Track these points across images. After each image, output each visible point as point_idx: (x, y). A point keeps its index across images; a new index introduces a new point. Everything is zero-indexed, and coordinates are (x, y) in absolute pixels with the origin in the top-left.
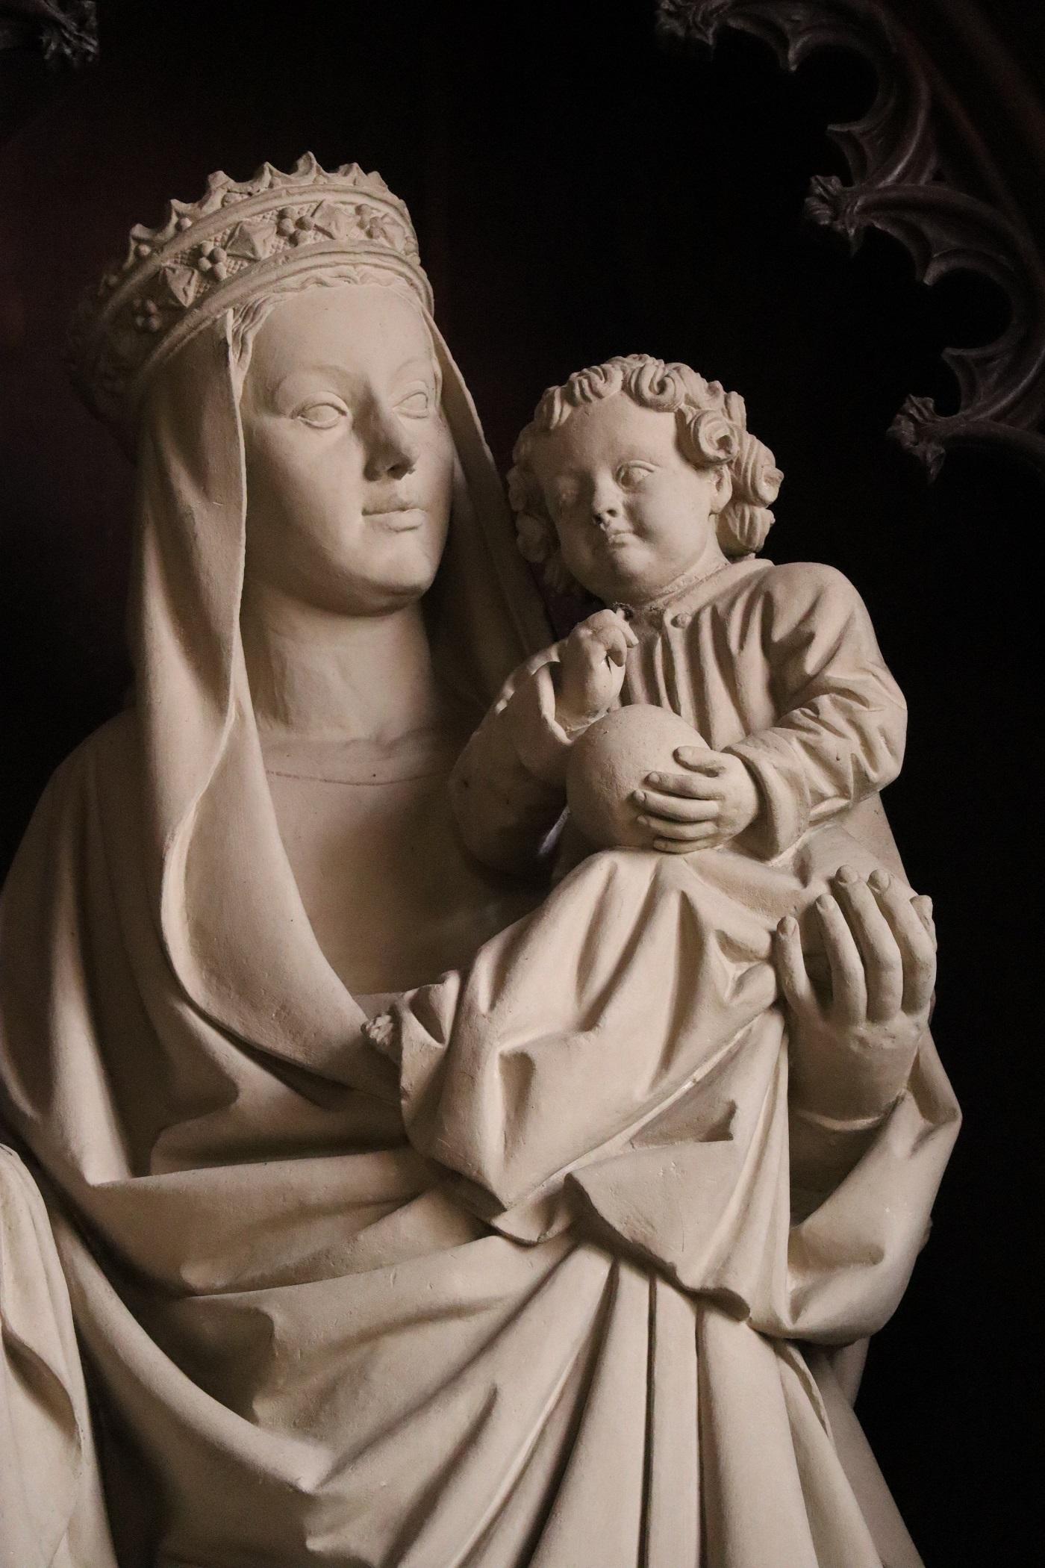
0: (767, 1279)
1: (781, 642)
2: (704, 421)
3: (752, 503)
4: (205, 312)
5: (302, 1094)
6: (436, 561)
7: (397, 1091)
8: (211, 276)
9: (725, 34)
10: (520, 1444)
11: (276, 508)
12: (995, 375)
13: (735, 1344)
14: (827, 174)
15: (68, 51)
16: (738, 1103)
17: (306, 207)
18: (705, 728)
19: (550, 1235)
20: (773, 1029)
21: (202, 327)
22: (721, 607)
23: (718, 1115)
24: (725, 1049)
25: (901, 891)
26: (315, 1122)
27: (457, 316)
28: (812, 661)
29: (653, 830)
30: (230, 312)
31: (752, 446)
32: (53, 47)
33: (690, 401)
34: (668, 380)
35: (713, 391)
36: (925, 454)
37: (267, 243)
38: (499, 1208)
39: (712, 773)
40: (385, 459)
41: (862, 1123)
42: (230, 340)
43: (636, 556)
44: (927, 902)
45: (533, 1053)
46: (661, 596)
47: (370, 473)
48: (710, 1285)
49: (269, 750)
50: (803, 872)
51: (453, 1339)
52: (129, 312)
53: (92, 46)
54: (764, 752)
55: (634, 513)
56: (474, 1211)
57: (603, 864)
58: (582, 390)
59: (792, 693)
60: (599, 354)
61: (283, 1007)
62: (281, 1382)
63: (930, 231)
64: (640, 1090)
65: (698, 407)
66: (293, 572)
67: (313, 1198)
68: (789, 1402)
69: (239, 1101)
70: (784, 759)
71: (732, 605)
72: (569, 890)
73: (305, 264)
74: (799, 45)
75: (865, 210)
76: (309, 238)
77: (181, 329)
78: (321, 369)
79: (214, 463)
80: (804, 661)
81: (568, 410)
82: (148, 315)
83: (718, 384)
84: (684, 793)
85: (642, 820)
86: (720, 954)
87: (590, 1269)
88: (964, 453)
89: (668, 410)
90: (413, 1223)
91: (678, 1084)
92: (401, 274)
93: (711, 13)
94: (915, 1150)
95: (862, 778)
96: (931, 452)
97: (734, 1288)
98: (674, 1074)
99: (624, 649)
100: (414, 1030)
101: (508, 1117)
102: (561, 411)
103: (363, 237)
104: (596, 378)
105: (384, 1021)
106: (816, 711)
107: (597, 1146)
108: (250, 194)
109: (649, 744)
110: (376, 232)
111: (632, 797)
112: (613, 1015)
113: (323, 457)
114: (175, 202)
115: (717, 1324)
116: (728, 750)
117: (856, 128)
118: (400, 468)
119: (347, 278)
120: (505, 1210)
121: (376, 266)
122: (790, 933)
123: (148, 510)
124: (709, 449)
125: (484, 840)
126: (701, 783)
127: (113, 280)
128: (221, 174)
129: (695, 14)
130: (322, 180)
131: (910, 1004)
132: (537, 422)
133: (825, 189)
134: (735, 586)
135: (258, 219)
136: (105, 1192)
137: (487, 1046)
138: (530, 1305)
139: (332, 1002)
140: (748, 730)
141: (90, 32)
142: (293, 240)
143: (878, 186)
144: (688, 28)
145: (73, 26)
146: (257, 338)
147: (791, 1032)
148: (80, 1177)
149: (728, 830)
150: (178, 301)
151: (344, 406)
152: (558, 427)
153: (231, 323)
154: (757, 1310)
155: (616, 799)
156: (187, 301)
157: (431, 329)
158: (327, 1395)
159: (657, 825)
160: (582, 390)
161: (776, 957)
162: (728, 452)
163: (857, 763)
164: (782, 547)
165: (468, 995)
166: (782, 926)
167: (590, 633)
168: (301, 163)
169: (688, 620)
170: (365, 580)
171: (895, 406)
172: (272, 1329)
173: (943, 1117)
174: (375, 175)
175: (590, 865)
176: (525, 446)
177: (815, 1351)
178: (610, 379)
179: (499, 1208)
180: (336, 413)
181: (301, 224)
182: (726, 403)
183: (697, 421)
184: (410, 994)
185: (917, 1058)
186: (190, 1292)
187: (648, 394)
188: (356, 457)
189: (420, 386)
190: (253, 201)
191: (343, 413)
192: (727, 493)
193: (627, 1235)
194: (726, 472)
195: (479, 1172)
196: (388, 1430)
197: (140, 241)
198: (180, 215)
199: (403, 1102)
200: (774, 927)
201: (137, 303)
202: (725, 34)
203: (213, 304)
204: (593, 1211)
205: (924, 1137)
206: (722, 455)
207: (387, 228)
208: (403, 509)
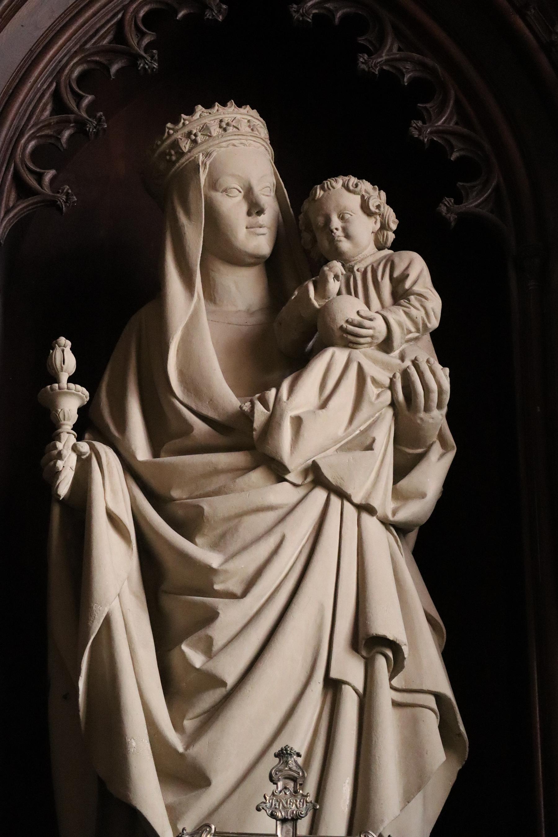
0: (383, 501)
1: (397, 277)
2: (371, 199)
3: (387, 230)
4: (192, 154)
5: (215, 430)
6: (272, 248)
7: (252, 429)
8: (195, 142)
9: (382, 71)
10: (293, 555)
11: (214, 223)
12: (475, 193)
13: (371, 524)
14: (417, 119)
15: (147, 67)
16: (376, 438)
17: (230, 119)
18: (367, 303)
19: (306, 482)
20: (390, 413)
21: (191, 159)
22: (375, 265)
23: (368, 442)
24: (372, 419)
25: (438, 367)
26: (221, 440)
27: (281, 162)
28: (408, 284)
29: (348, 339)
30: (201, 155)
31: (388, 210)
32: (142, 65)
33: (366, 192)
34: (359, 183)
35: (374, 189)
36: (450, 217)
37: (215, 130)
38: (287, 471)
39: (371, 320)
40: (254, 208)
41: (420, 451)
42: (200, 164)
43: (345, 245)
44: (447, 370)
45: (302, 416)
46: (353, 261)
47: (249, 214)
48: (363, 502)
49: (208, 312)
50: (402, 358)
51: (270, 517)
52: (164, 154)
53: (156, 65)
54: (389, 315)
55: (345, 230)
56: (278, 472)
57: (330, 351)
58: (327, 185)
59: (400, 295)
60: (335, 174)
61: (211, 400)
62: (206, 531)
63: (454, 142)
64: (341, 432)
65: (369, 194)
66: (221, 247)
67: (220, 467)
68: (390, 546)
69: (194, 432)
70: (397, 316)
71: (379, 264)
72: (319, 356)
73: (229, 138)
74: (408, 76)
75: (431, 133)
76: (230, 129)
77: (183, 160)
78: (233, 175)
79: (193, 207)
80: (405, 284)
81: (322, 193)
82: (171, 155)
83: (376, 187)
84: (361, 326)
85: (345, 335)
86: (372, 385)
87: (320, 495)
88: (463, 218)
89: (359, 194)
90: (257, 476)
91: (355, 431)
92: (263, 145)
93: (378, 63)
94: (439, 459)
95: (425, 325)
96: (452, 217)
97: (372, 504)
98: (356, 423)
99: (340, 275)
100: (259, 407)
101: (292, 439)
102: (319, 193)
103: (250, 131)
104: (333, 182)
105: (248, 404)
106: (409, 301)
107: (324, 451)
108: (210, 113)
109: (348, 309)
110: (255, 129)
111: (341, 327)
112: (332, 404)
113: (233, 207)
114: (183, 115)
115: (365, 516)
116: (377, 312)
117: (428, 105)
118: (260, 212)
119: (244, 145)
120: (290, 472)
121: (254, 141)
122: (397, 378)
123: (168, 225)
124: (373, 209)
125: (285, 342)
126: (367, 323)
127: (159, 143)
128: (200, 106)
129: (372, 63)
130: (236, 110)
131: (439, 407)
132: (310, 198)
133: (417, 126)
134: (380, 258)
135: (212, 122)
136: (144, 463)
137: (286, 413)
138: (296, 509)
139: (227, 397)
140: (383, 306)
141: (155, 61)
142: (225, 130)
143: (434, 125)
144: (369, 68)
145: (149, 59)
146: (210, 164)
147: (396, 416)
148: (134, 457)
149: (376, 341)
150: (181, 149)
151: (241, 190)
152: (318, 199)
153: (201, 158)
154: (380, 512)
155: (336, 328)
156: (186, 150)
157: (273, 166)
158: (223, 536)
159: (350, 337)
160: (327, 185)
161: (392, 387)
162: (380, 210)
163: (423, 320)
164: (396, 246)
165: (279, 395)
166: (394, 376)
167: (328, 268)
168: (229, 104)
169: (363, 270)
170: (245, 252)
171: (440, 201)
172: (204, 512)
173: (449, 449)
174: (255, 110)
175: (325, 351)
176: (306, 205)
177: (400, 529)
178: (338, 183)
179: (287, 471)
180: (238, 192)
181: (228, 124)
182: (379, 194)
183: (369, 198)
184: (258, 395)
185: (441, 428)
186: (173, 500)
187: (351, 188)
188: (244, 208)
189: (268, 185)
190: (211, 115)
191: (240, 192)
192: (378, 225)
193: (334, 483)
194: (378, 218)
195: (281, 458)
196: (245, 548)
197: (169, 129)
198: (184, 120)
199: (254, 433)
200: (391, 377)
201: (168, 151)
202: (382, 71)
203: (195, 151)
204: (322, 474)
205: (442, 456)
206: (377, 211)
207: (259, 129)
208: (261, 227)
